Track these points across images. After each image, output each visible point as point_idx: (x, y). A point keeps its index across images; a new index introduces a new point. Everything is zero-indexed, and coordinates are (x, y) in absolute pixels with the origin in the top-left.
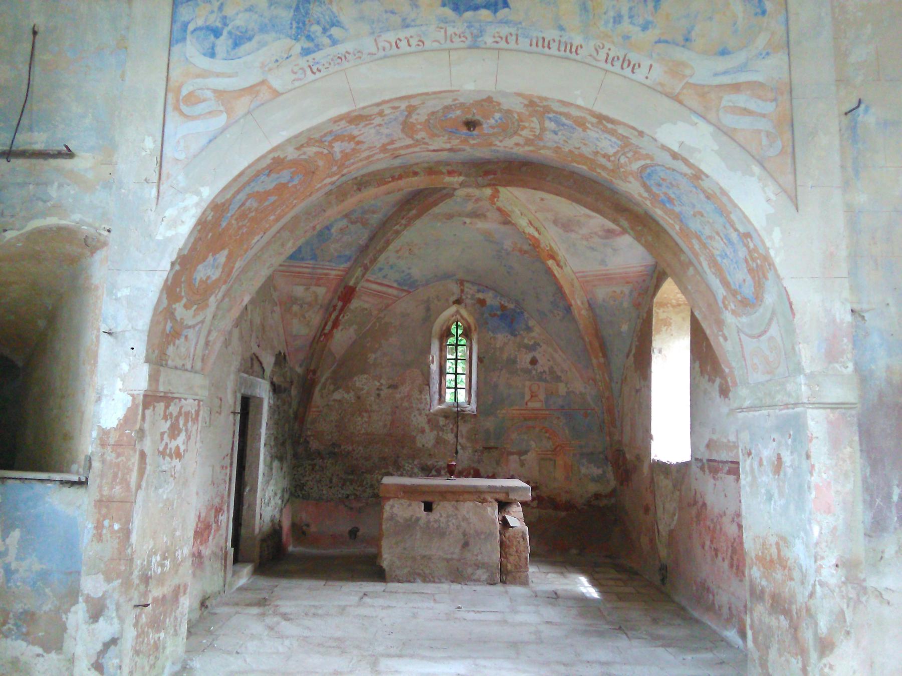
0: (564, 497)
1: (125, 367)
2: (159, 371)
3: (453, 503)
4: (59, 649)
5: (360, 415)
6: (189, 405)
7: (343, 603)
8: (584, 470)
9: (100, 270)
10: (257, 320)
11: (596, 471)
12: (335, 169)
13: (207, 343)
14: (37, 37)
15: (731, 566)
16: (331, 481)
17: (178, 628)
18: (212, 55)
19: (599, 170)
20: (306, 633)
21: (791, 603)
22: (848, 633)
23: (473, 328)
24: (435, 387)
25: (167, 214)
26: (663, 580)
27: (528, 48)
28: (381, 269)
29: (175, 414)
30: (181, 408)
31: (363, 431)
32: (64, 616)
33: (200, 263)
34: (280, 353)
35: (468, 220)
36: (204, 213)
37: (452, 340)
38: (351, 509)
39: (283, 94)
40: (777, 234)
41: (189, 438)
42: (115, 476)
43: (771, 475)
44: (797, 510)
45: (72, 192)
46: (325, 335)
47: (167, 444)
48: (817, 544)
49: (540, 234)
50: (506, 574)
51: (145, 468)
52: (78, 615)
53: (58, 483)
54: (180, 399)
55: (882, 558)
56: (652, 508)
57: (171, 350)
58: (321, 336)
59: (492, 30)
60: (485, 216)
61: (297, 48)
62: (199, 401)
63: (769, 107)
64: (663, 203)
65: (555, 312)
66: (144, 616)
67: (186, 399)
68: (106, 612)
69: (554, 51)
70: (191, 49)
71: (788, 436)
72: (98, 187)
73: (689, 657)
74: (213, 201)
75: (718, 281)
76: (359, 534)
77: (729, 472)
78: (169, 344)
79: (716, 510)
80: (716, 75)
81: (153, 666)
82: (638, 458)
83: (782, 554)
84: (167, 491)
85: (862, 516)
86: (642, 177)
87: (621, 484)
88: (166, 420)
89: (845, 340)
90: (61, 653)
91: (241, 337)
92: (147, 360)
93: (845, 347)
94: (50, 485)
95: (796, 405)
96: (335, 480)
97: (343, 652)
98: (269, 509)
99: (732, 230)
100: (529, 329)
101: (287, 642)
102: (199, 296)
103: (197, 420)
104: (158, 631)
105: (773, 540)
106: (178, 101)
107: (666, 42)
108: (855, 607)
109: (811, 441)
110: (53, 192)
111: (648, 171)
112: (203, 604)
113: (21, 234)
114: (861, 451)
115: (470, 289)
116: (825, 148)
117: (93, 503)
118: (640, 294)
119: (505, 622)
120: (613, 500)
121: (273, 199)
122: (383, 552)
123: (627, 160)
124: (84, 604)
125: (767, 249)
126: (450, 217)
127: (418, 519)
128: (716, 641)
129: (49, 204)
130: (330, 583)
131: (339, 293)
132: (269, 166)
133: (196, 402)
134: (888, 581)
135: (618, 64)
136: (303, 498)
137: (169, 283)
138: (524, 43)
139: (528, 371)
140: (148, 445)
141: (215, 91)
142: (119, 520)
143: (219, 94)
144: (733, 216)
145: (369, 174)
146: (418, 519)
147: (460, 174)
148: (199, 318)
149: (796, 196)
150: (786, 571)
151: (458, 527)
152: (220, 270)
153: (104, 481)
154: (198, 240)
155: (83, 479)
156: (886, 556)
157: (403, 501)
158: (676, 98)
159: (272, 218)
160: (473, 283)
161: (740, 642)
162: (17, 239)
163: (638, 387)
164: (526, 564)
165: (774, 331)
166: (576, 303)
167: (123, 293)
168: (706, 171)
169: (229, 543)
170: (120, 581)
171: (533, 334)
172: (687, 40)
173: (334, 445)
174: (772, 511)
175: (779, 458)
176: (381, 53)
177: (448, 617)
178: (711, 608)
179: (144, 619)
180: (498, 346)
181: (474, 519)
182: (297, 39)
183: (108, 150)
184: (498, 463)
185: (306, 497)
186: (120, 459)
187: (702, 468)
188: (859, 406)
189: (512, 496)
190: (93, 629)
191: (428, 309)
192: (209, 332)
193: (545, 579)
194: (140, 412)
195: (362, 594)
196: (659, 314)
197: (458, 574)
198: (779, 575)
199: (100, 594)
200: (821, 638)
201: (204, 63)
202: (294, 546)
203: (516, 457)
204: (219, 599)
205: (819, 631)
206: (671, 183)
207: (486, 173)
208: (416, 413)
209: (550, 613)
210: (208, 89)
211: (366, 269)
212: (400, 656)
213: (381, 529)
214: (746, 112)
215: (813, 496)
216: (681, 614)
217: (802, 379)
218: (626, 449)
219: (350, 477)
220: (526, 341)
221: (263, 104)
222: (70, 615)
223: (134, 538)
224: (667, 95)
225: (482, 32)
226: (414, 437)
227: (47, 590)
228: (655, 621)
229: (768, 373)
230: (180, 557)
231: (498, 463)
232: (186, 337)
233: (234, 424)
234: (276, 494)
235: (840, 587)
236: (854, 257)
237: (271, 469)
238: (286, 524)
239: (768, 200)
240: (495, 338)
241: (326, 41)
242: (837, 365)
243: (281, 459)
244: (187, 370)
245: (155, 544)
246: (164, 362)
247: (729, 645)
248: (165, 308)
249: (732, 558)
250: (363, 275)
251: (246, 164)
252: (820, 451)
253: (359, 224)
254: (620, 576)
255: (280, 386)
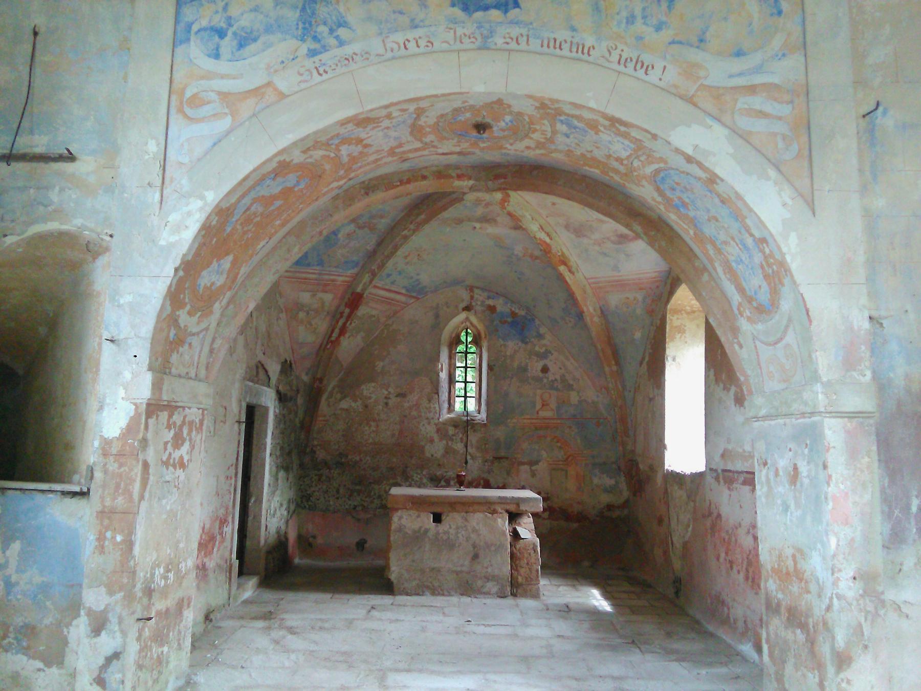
0: (576, 508)
1: (128, 375)
2: (162, 379)
3: (463, 514)
4: (60, 663)
5: (368, 424)
6: (193, 414)
7: (351, 617)
8: (596, 481)
9: (102, 276)
10: (263, 328)
11: (609, 482)
12: (342, 172)
13: (211, 351)
14: (38, 38)
15: (747, 578)
16: (338, 492)
17: (181, 642)
18: (217, 56)
19: (611, 174)
20: (313, 647)
21: (807, 616)
22: (866, 647)
23: (483, 335)
24: (444, 396)
25: (170, 219)
26: (677, 593)
27: (539, 49)
28: (389, 275)
29: (178, 423)
30: (185, 417)
31: (371, 440)
32: (65, 630)
33: (203, 269)
34: (286, 361)
35: (478, 225)
36: (208, 218)
37: (461, 348)
38: (359, 520)
39: (288, 96)
40: (793, 239)
41: (193, 447)
42: (118, 487)
43: (787, 486)
44: (813, 522)
45: (74, 196)
46: (332, 342)
47: (170, 454)
48: (834, 556)
49: (551, 239)
50: (517, 587)
51: (148, 478)
52: (79, 629)
53: (59, 493)
54: (184, 408)
55: (900, 570)
56: (666, 520)
57: (174, 358)
58: (327, 343)
59: (502, 30)
60: (495, 221)
61: (304, 49)
62: (203, 410)
63: (786, 110)
64: (677, 208)
65: (567, 318)
66: (147, 630)
67: (190, 408)
68: (108, 626)
69: (566, 52)
70: (195, 50)
71: (804, 446)
72: (101, 192)
73: (703, 672)
74: (217, 205)
75: (733, 287)
76: (367, 545)
77: (745, 483)
78: (172, 351)
79: (731, 521)
80: (731, 76)
81: (156, 681)
82: (652, 468)
83: (799, 566)
84: (170, 502)
85: (881, 528)
86: (655, 181)
87: (634, 495)
88: (170, 429)
89: (863, 348)
90: (62, 668)
91: (246, 344)
92: (150, 368)
93: (863, 355)
94: (51, 495)
95: (812, 414)
96: (342, 490)
97: (350, 667)
98: (275, 520)
99: (747, 235)
100: (540, 336)
101: (293, 657)
102: (204, 302)
103: (202, 429)
104: (162, 645)
105: (789, 552)
106: (181, 103)
107: (680, 43)
108: (873, 621)
109: (828, 450)
110: (54, 196)
111: (662, 174)
112: (207, 618)
113: (22, 240)
114: (879, 461)
115: (479, 295)
116: (842, 150)
117: (95, 514)
118: (653, 301)
119: (515, 636)
120: (626, 512)
121: (278, 203)
122: (391, 564)
123: (640, 163)
124: (86, 618)
125: (783, 255)
126: (459, 221)
127: (427, 531)
128: (731, 656)
129: (50, 209)
130: (337, 596)
131: (346, 300)
132: (274, 170)
133: (201, 411)
134: (907, 593)
135: (631, 65)
136: (309, 509)
137: (173, 289)
138: (535, 44)
139: (539, 380)
140: (151, 455)
141: (219, 93)
142: (121, 532)
143: (224, 96)
144: (748, 221)
145: (377, 178)
146: (427, 531)
147: (470, 178)
148: (203, 325)
149: (813, 200)
150: (803, 584)
151: (468, 539)
152: (225, 276)
153: (106, 492)
154: (203, 245)
155: (85, 490)
156: (905, 568)
157: (411, 512)
158: (690, 100)
159: (278, 222)
160: (483, 289)
161: (755, 656)
162: (18, 244)
163: (651, 396)
164: (538, 577)
165: (790, 338)
166: (588, 309)
167: (126, 299)
168: (721, 175)
169: (234, 555)
170: (122, 594)
171: (544, 342)
172: (701, 41)
173: (341, 455)
174: (788, 522)
175: (795, 468)
176: (389, 55)
177: (458, 631)
178: (726, 622)
179: (147, 633)
180: (508, 354)
181: (484, 531)
182: (303, 40)
183: (110, 153)
184: (508, 473)
185: (312, 508)
186: (122, 469)
187: (717, 479)
188: (877, 415)
189: (523, 507)
190: (95, 643)
191: (437, 316)
192: (214, 340)
193: (557, 592)
194: (143, 421)
195: (369, 607)
196: (673, 320)
197: (467, 587)
198: (795, 588)
199: (102, 607)
200: (838, 653)
201: (208, 64)
202: (301, 558)
203: (527, 467)
204: (223, 612)
205: (836, 645)
206: (685, 188)
207: (497, 177)
208: (425, 422)
209: (562, 627)
210: (213, 91)
211: (374, 275)
212: (408, 671)
213: (389, 541)
214: (762, 114)
215: (830, 506)
216: (696, 628)
217: (818, 387)
218: (639, 459)
219: (358, 487)
220: (537, 348)
221: (268, 107)
222: (72, 629)
223: (137, 550)
224: (681, 97)
225: (492, 32)
226: (423, 447)
227: (48, 603)
228: (669, 635)
229: (785, 381)
230: (183, 569)
231: (508, 473)
232: (190, 344)
233: (239, 434)
234: (281, 505)
235: (858, 601)
236: (872, 263)
237: (277, 480)
238: (292, 536)
239: (784, 205)
240: (505, 346)
241: (332, 41)
242: (855, 374)
243: (287, 469)
244: (191, 378)
245: (158, 556)
246: (167, 371)
247: (744, 659)
248: (168, 315)
249: (747, 571)
250: (371, 282)
251: (251, 168)
252: (837, 461)
253: (366, 229)
254: (633, 589)
255: (285, 395)
